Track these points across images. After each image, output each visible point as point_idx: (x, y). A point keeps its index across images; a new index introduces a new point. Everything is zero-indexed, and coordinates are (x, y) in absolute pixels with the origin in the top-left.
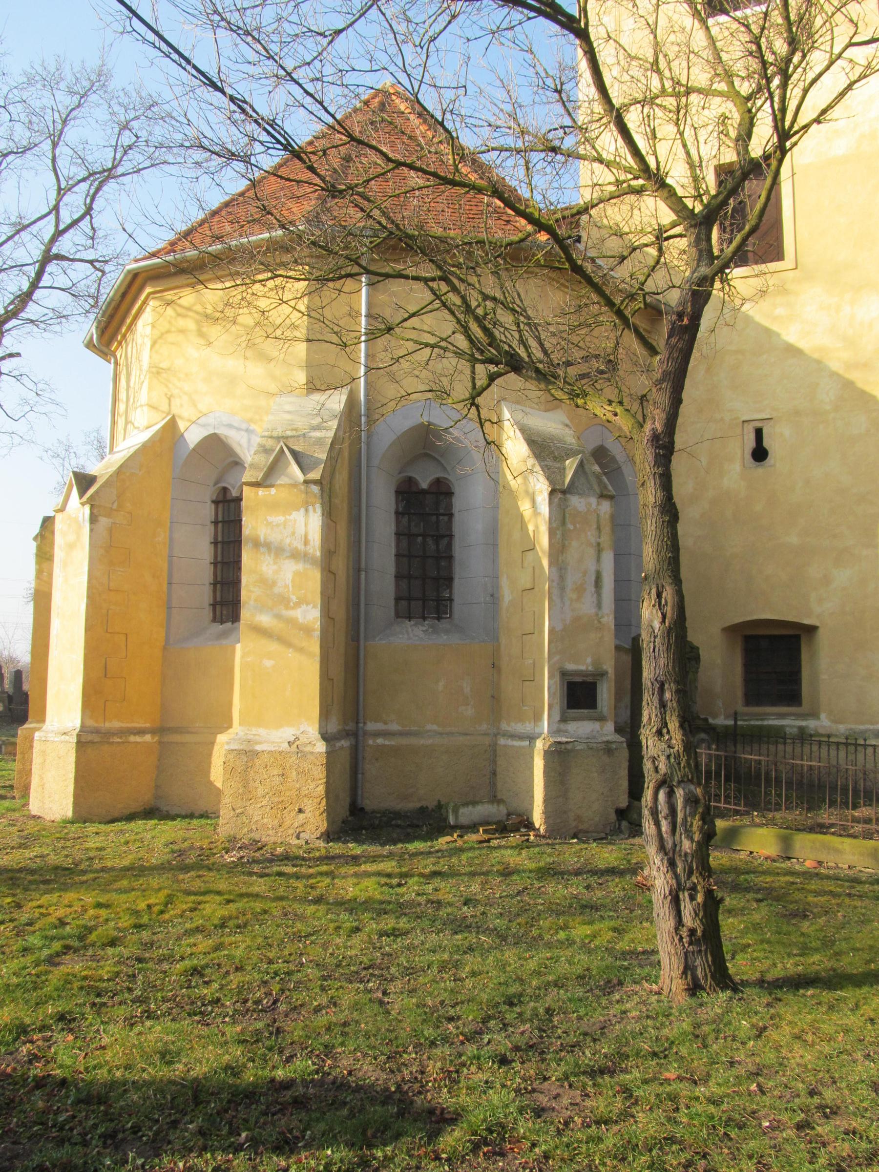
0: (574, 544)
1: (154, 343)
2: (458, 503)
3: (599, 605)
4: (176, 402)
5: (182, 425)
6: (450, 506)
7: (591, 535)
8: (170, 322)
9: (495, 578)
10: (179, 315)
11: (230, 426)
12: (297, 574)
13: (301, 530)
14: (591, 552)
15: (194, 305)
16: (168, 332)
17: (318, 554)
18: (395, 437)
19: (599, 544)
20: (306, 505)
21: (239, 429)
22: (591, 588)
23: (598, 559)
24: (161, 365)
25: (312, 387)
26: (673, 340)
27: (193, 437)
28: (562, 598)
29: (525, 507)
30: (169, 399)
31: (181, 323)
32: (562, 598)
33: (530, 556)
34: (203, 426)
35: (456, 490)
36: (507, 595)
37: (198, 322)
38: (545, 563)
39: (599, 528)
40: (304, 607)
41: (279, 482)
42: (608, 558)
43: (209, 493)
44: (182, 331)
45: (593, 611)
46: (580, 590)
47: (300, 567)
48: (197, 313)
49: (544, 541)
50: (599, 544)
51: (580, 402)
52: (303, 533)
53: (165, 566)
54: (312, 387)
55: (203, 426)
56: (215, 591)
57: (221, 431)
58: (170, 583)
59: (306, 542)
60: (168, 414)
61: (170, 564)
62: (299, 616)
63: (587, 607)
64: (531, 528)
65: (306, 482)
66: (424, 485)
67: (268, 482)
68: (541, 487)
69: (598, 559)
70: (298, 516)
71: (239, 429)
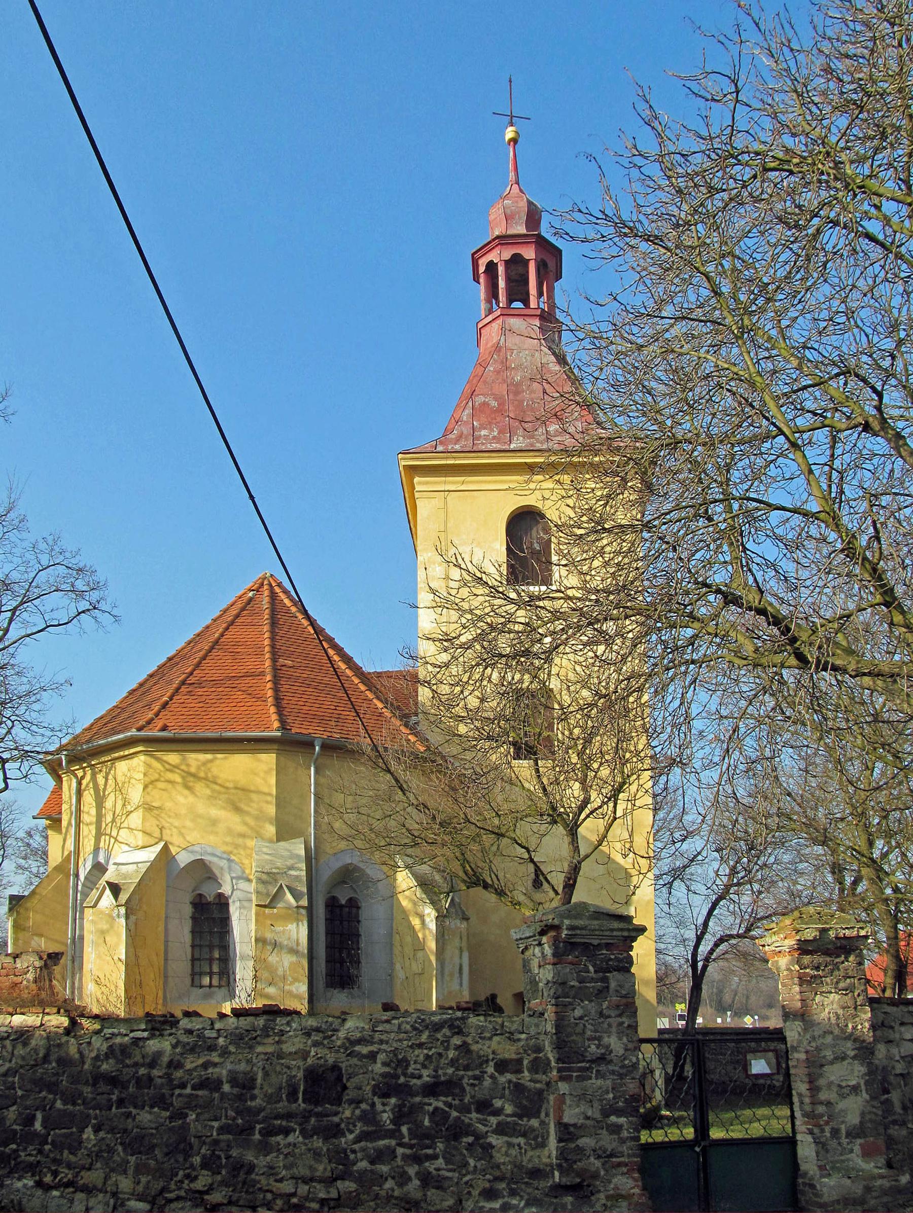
0: (449, 947)
1: (145, 787)
2: (364, 914)
3: (461, 985)
4: (166, 832)
5: (173, 850)
6: (357, 915)
7: (457, 943)
8: (160, 775)
9: (392, 964)
10: (167, 770)
11: (214, 855)
12: (291, 963)
13: (294, 936)
14: (457, 952)
15: (181, 764)
16: (157, 780)
17: (306, 951)
18: (330, 873)
19: (461, 948)
20: (298, 920)
21: (221, 858)
22: (457, 975)
23: (461, 958)
24: (154, 804)
25: (281, 836)
26: (566, 890)
27: (184, 859)
28: (442, 980)
29: (416, 922)
30: (161, 830)
31: (169, 776)
32: (442, 980)
33: (420, 954)
34: (192, 852)
35: (363, 904)
36: (400, 974)
37: (183, 778)
38: (433, 959)
39: (461, 938)
40: (297, 984)
41: (279, 905)
42: (466, 955)
43: (188, 898)
44: (169, 781)
45: (458, 987)
46: (451, 975)
47: (294, 959)
48: (183, 770)
49: (432, 945)
50: (461, 948)
51: (517, 907)
52: (295, 937)
53: (162, 948)
54: (281, 836)
55: (192, 852)
56: (193, 965)
57: (207, 858)
58: (166, 960)
59: (298, 944)
60: (161, 840)
61: (166, 947)
62: (294, 990)
63: (455, 986)
64: (420, 935)
65: (298, 907)
66: (343, 902)
67: (274, 905)
68: (430, 913)
69: (461, 958)
70: (292, 927)
71: (221, 858)
